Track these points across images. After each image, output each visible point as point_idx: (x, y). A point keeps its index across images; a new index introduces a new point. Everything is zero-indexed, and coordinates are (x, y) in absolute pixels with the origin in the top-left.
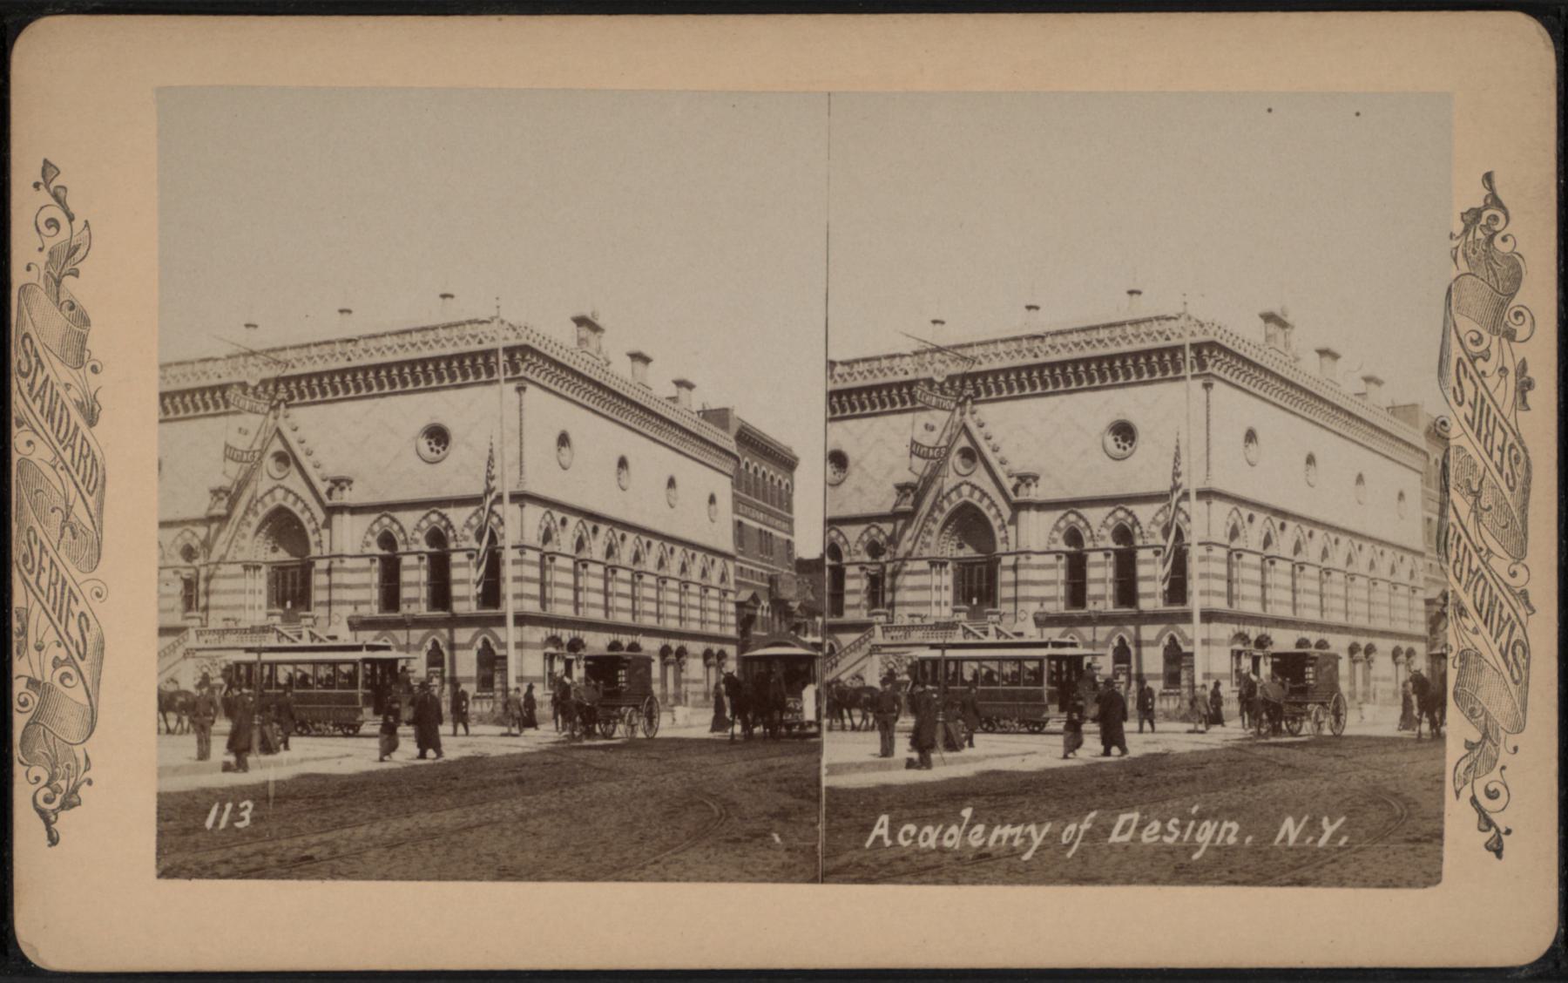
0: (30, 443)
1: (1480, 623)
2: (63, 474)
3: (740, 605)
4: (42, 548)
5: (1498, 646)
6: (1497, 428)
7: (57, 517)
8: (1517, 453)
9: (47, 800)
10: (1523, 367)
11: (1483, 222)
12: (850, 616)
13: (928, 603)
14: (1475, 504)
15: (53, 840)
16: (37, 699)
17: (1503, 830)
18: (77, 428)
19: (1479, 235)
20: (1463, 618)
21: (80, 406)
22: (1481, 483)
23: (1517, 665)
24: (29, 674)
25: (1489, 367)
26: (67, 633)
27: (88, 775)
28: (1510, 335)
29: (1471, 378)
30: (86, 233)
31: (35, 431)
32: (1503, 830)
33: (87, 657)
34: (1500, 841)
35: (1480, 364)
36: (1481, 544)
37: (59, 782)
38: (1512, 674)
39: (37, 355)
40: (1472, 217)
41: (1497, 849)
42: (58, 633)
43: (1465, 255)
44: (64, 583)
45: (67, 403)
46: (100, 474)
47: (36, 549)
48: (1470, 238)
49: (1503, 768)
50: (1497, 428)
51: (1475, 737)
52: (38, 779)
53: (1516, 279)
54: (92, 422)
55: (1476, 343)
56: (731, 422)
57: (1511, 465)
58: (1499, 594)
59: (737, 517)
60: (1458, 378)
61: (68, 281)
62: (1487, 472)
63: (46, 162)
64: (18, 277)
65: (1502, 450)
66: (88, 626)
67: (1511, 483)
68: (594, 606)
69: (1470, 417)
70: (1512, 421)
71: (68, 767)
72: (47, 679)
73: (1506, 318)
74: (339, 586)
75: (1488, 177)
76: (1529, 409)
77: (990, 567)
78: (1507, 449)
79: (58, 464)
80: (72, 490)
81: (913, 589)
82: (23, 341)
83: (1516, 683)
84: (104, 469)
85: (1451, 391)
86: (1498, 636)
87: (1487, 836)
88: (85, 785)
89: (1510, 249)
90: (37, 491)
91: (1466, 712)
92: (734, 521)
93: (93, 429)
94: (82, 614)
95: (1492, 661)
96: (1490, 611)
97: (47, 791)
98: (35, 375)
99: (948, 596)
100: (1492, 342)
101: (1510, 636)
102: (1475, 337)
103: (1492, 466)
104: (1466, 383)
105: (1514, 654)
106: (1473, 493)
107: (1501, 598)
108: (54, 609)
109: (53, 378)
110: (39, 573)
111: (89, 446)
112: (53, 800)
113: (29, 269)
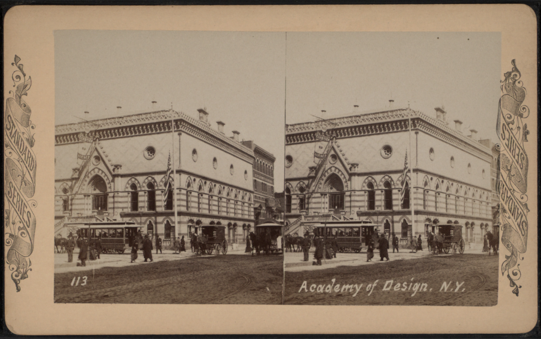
0: (10, 153)
1: (511, 215)
2: (22, 163)
3: (255, 209)
5: (517, 222)
6: (517, 147)
7: (20, 178)
8: (523, 156)
9: (16, 276)
10: (525, 126)
11: (512, 76)
12: (293, 212)
13: (320, 208)
15: (18, 290)
16: (13, 241)
17: (519, 286)
18: (26, 148)
21: (28, 140)
22: (511, 167)
25: (514, 127)
26: (23, 218)
27: (30, 267)
28: (521, 116)
29: (508, 130)
30: (30, 80)
32: (519, 286)
33: (30, 227)
34: (517, 290)
35: (511, 125)
36: (511, 188)
37: (20, 270)
38: (522, 233)
39: (13, 123)
40: (508, 75)
41: (516, 293)
43: (505, 88)
44: (22, 201)
45: (23, 139)
46: (35, 164)
48: (507, 82)
49: (519, 265)
50: (517, 147)
51: (509, 254)
52: (13, 269)
53: (523, 96)
55: (509, 118)
56: (252, 146)
61: (24, 97)
63: (16, 56)
64: (6, 95)
65: (518, 155)
66: (30, 216)
67: (521, 166)
68: (205, 209)
69: (507, 144)
70: (522, 145)
71: (23, 264)
72: (16, 234)
73: (520, 110)
74: (117, 202)
75: (513, 61)
76: (527, 141)
77: (342, 195)
78: (520, 155)
79: (20, 160)
81: (315, 203)
83: (523, 235)
86: (517, 219)
88: (29, 271)
90: (13, 169)
92: (253, 180)
94: (28, 212)
96: (514, 211)
97: (16, 273)
98: (12, 129)
99: (327, 205)
100: (515, 118)
101: (521, 220)
103: (515, 161)
105: (522, 225)
106: (508, 170)
107: (15, 145)
108: (19, 210)
109: (18, 130)
110: (14, 198)
111: (31, 154)
112: (514, 75)
113: (10, 93)
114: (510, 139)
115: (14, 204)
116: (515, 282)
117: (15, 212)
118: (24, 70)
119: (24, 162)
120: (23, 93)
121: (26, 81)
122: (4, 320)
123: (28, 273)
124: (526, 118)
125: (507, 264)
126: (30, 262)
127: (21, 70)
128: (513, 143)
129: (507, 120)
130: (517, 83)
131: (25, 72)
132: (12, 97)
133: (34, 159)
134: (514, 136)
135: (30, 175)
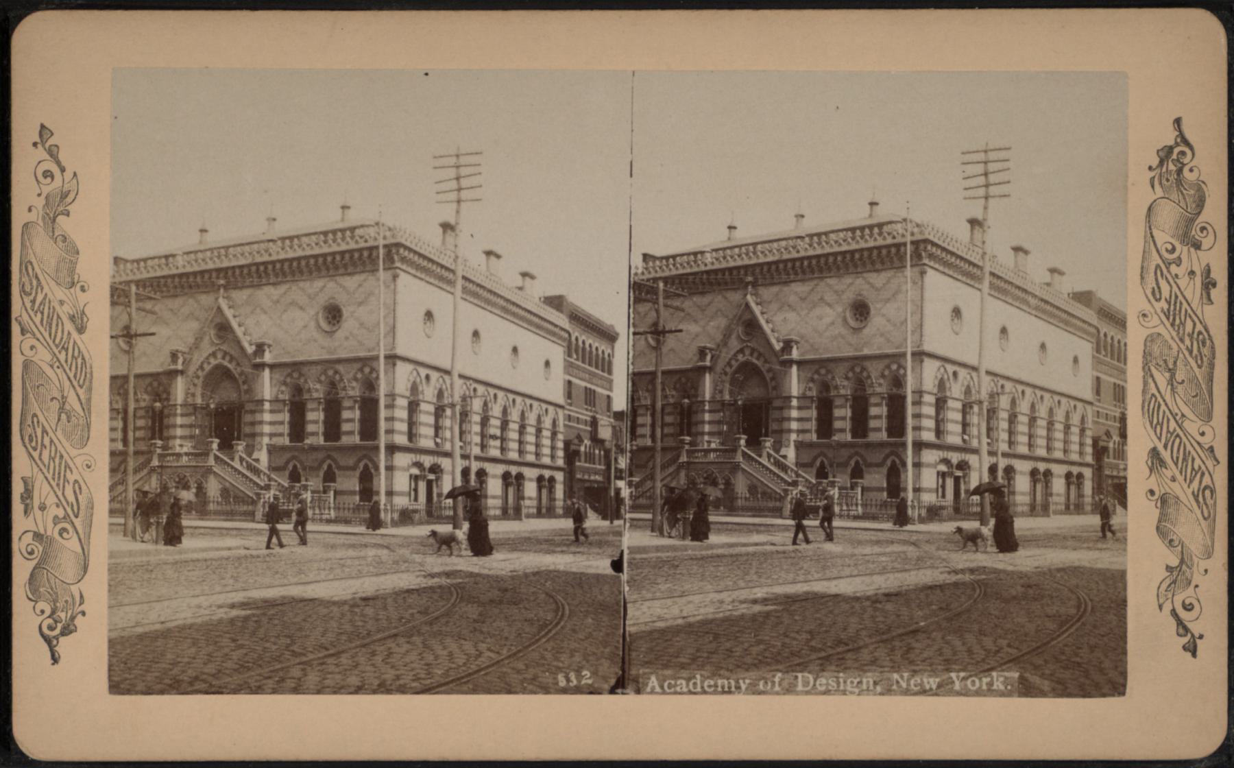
0: (1203, 434)
1: (58, 308)
2: (59, 371)
5: (1191, 490)
6: (47, 463)
7: (55, 405)
8: (1203, 338)
9: (1183, 153)
10: (1208, 271)
11: (1174, 156)
15: (55, 659)
16: (41, 549)
17: (1197, 635)
18: (1165, 447)
19: (63, 615)
20: (1164, 470)
21: (72, 318)
22: (1175, 363)
23: (1206, 504)
25: (54, 511)
27: (1152, 174)
28: (1197, 246)
29: (68, 503)
30: (75, 181)
31: (1199, 443)
32: (1197, 635)
35: (1173, 268)
36: (1176, 411)
37: (59, 613)
38: (1202, 513)
39: (37, 277)
40: (1166, 154)
41: (1192, 649)
42: (57, 496)
43: (1161, 183)
46: (88, 370)
47: (39, 431)
48: (1164, 169)
49: (1197, 586)
50: (47, 463)
51: (1175, 562)
52: (43, 612)
53: (1201, 203)
54: (81, 330)
55: (64, 530)
57: (1199, 347)
58: (1192, 450)
59: (568, 377)
60: (1157, 279)
61: (1175, 562)
62: (54, 428)
63: (43, 126)
64: (19, 216)
65: (43, 446)
66: (80, 488)
67: (35, 419)
69: (68, 471)
71: (1168, 180)
72: (49, 533)
73: (1193, 232)
75: (1178, 121)
76: (1212, 303)
78: (1195, 336)
79: (56, 363)
80: (1168, 397)
82: (1209, 516)
83: (1205, 519)
84: (1143, 414)
85: (83, 491)
86: (1191, 481)
87: (51, 142)
88: (80, 615)
91: (1166, 542)
92: (565, 380)
93: (1152, 446)
94: (76, 481)
96: (50, 318)
97: (50, 621)
98: (36, 293)
101: (1201, 482)
102: (1170, 247)
103: (51, 434)
104: (71, 498)
105: (1204, 496)
107: (1193, 452)
108: (1181, 303)
109: (50, 295)
112: (1179, 153)
113: (30, 210)
114: (1173, 301)
116: (1190, 625)
117: (45, 482)
118: (61, 157)
119: (1172, 414)
120: (61, 209)
123: (76, 622)
124: (26, 532)
125: (67, 196)
126: (81, 596)
127: (1180, 622)
128: (54, 474)
130: (1186, 171)
131: (63, 164)
132: (1201, 561)
133: (1148, 423)
134: (1182, 293)
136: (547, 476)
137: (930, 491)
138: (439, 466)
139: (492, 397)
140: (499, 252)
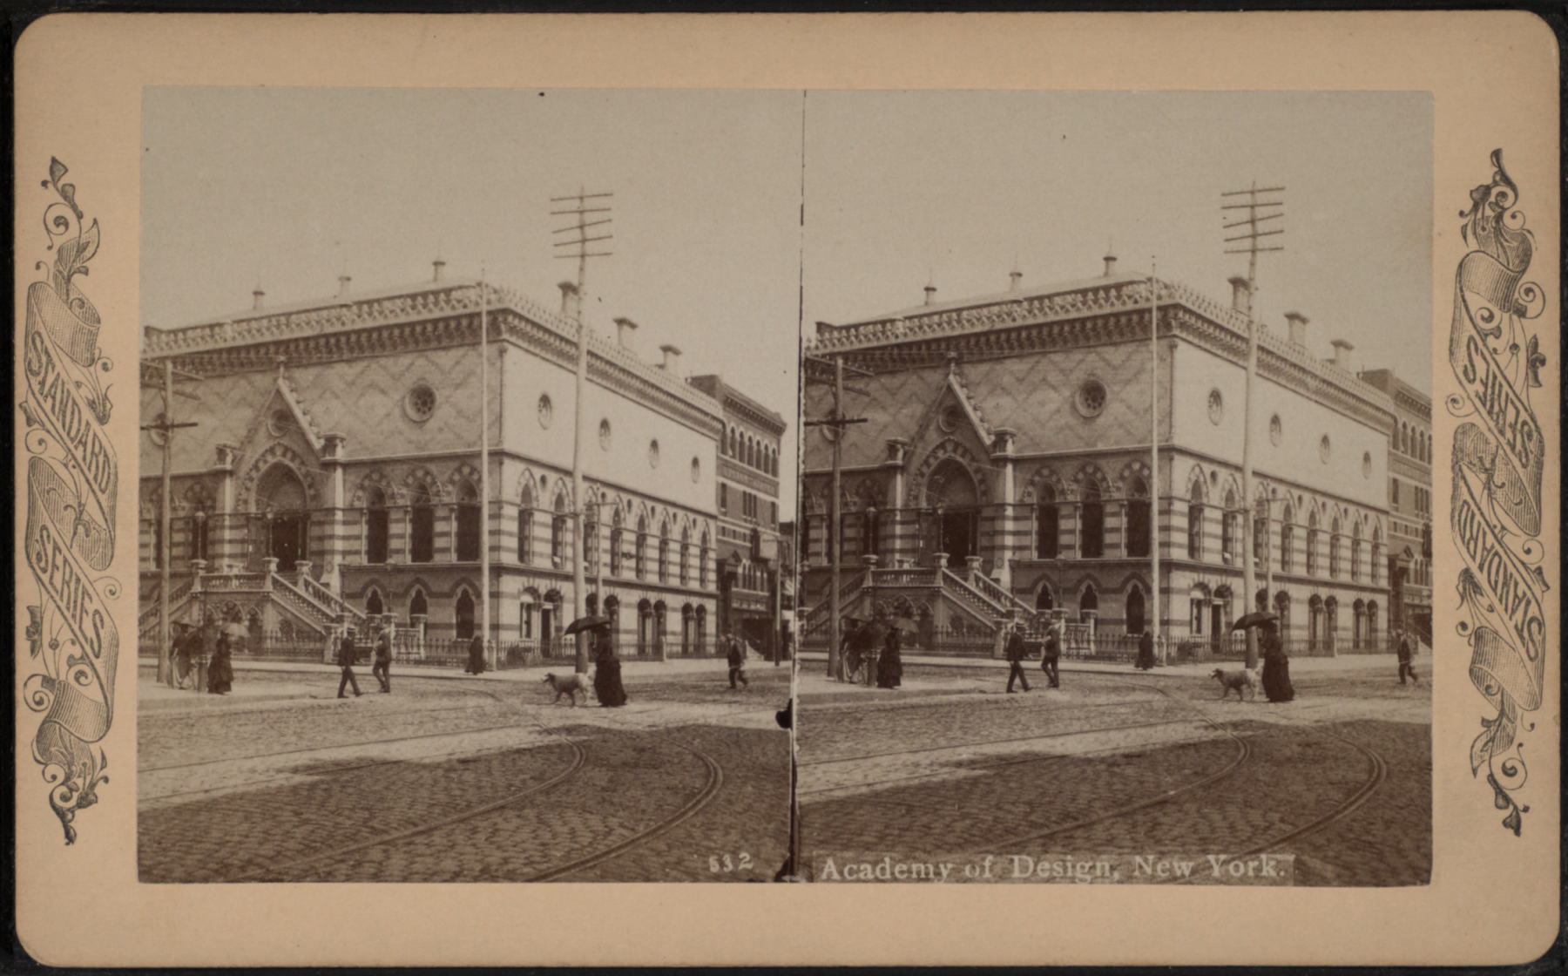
0: (1528, 552)
2: (75, 472)
4: (1513, 447)
5: (1513, 623)
7: (70, 515)
8: (1529, 429)
9: (1503, 195)
10: (1535, 344)
11: (1492, 199)
14: (81, 513)
15: (70, 838)
16: (52, 697)
17: (1521, 807)
18: (1481, 568)
19: (80, 782)
20: (1479, 597)
21: (92, 404)
22: (1493, 461)
23: (1532, 641)
24: (44, 672)
26: (82, 631)
27: (1464, 221)
28: (1521, 313)
29: (86, 639)
30: (95, 230)
31: (1523, 564)
33: (102, 655)
34: (1518, 817)
35: (1491, 341)
36: (1495, 522)
37: (75, 779)
38: (1528, 651)
39: (47, 352)
40: (1481, 195)
41: (1515, 825)
42: (72, 630)
43: (1475, 233)
44: (78, 580)
45: (79, 401)
46: (112, 471)
47: (50, 548)
48: (1479, 215)
50: (1510, 405)
51: (1492, 714)
52: (54, 777)
53: (1526, 258)
54: (103, 419)
55: (81, 673)
57: (1523, 441)
59: (721, 480)
60: (1469, 355)
62: (68, 544)
63: (54, 161)
64: (24, 275)
65: (55, 566)
66: (102, 621)
67: (45, 533)
70: (45, 596)
71: (1484, 229)
72: (62, 677)
73: (1516, 295)
75: (1496, 154)
78: (1519, 426)
79: (71, 462)
80: (1484, 505)
83: (1531, 659)
85: (106, 625)
86: (1514, 612)
88: (101, 783)
89: (1518, 226)
90: (1520, 503)
91: (1482, 688)
92: (717, 483)
93: (1464, 566)
94: (97, 612)
95: (1509, 640)
96: (64, 405)
97: (64, 789)
100: (66, 675)
101: (1526, 613)
102: (1486, 314)
104: (91, 633)
105: (1529, 631)
106: (1486, 470)
107: (1516, 575)
108: (1501, 385)
109: (63, 375)
110: (52, 573)
111: (1468, 548)
112: (1498, 195)
113: (38, 267)
114: (1491, 382)
115: (1513, 403)
117: (58, 614)
118: (78, 199)
119: (1489, 525)
120: (77, 265)
121: (84, 231)
122: (14, 927)
123: (97, 790)
127: (1499, 791)
128: (68, 603)
129: (1482, 324)
131: (81, 208)
132: (1526, 713)
134: (1502, 372)
135: (1469, 489)
136: (695, 605)
137: (1181, 623)
138: (558, 593)
139: (625, 504)
140: (634, 320)
